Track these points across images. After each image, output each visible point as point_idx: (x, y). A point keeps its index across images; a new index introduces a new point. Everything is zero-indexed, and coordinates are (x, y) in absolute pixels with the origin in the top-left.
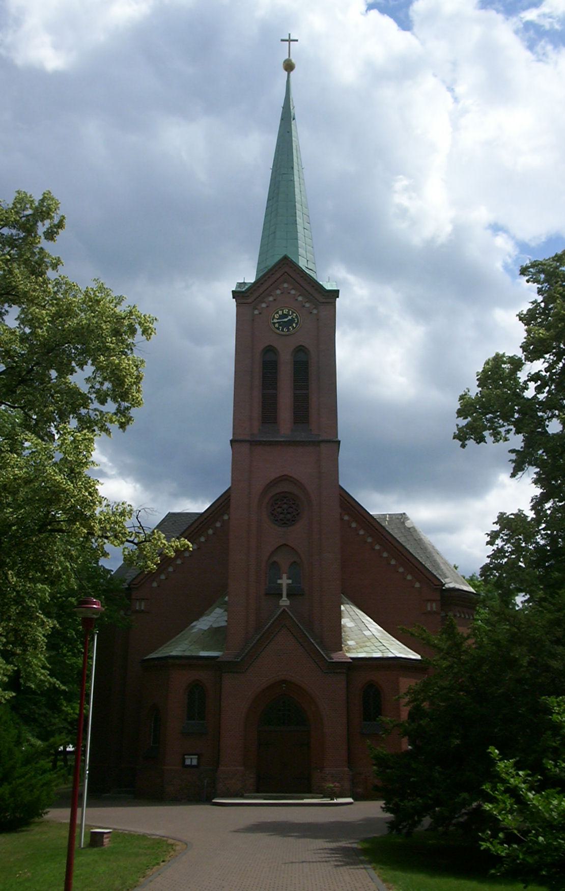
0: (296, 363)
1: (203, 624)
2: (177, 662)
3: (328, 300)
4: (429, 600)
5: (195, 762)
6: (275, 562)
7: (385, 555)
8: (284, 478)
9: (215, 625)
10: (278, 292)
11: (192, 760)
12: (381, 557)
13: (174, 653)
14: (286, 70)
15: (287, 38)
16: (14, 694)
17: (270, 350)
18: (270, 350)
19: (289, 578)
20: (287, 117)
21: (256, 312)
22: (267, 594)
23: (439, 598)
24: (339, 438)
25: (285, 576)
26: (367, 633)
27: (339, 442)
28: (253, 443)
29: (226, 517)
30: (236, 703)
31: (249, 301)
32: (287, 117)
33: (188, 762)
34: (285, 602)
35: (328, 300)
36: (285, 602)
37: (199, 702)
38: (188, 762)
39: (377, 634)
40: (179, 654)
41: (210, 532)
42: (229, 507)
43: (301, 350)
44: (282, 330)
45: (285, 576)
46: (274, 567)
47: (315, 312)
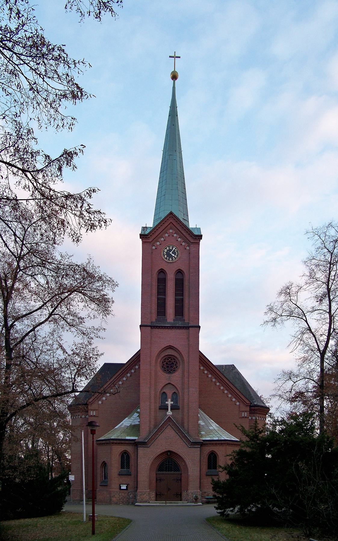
0: (176, 280)
1: (126, 422)
2: (115, 442)
3: (196, 241)
6: (164, 392)
8: (170, 347)
9: (133, 424)
10: (167, 235)
11: (124, 487)
15: (173, 55)
16: (239, 507)
18: (162, 271)
21: (154, 248)
22: (207, 475)
25: (169, 400)
26: (211, 428)
27: (199, 327)
29: (137, 367)
30: (146, 460)
31: (150, 240)
34: (169, 413)
35: (196, 241)
36: (169, 413)
37: (126, 460)
39: (216, 428)
40: (116, 438)
41: (129, 375)
42: (139, 361)
43: (179, 272)
44: (169, 260)
45: (169, 400)
47: (188, 248)
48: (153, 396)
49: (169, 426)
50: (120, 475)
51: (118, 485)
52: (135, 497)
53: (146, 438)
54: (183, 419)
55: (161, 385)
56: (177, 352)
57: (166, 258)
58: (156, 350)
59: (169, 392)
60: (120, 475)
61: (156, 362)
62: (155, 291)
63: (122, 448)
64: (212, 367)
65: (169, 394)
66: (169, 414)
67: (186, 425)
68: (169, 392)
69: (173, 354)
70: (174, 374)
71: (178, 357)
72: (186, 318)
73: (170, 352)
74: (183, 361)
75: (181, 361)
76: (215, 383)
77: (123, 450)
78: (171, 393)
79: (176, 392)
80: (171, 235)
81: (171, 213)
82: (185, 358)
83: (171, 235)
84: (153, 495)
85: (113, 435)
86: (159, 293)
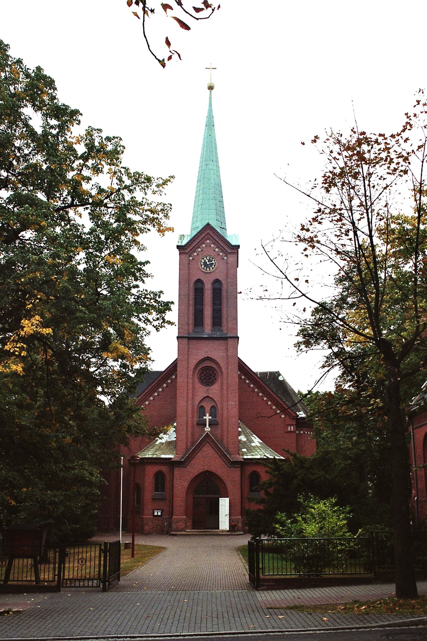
2: (150, 461)
4: (289, 425)
5: (159, 514)
6: (202, 406)
7: (265, 399)
10: (204, 246)
11: (158, 513)
12: (259, 395)
13: (147, 456)
14: (209, 89)
17: (199, 281)
19: (210, 416)
20: (210, 125)
21: (191, 258)
23: (295, 424)
24: (239, 335)
25: (207, 415)
26: (253, 444)
27: (238, 338)
28: (190, 338)
29: (174, 377)
30: (181, 482)
31: (187, 251)
32: (210, 125)
33: (156, 514)
34: (207, 429)
36: (207, 429)
37: (161, 481)
38: (156, 514)
43: (217, 281)
44: (206, 270)
45: (207, 415)
46: (201, 411)
47: (225, 258)
48: (190, 409)
49: (207, 444)
50: (154, 499)
51: (151, 511)
52: (170, 525)
53: (183, 458)
54: (222, 436)
55: (198, 399)
56: (216, 364)
57: (204, 269)
58: (193, 362)
59: (207, 406)
60: (154, 499)
61: (194, 372)
62: (192, 302)
63: (156, 468)
64: (253, 374)
65: (208, 408)
66: (207, 430)
67: (225, 441)
68: (207, 406)
69: (210, 365)
70: (211, 388)
71: (218, 370)
72: (224, 328)
73: (207, 364)
74: (221, 371)
75: (219, 373)
76: (258, 393)
77: (157, 470)
78: (209, 408)
79: (215, 405)
80: (208, 246)
81: (208, 224)
82: (223, 365)
83: (208, 246)
84: (190, 524)
85: (149, 454)
86: (196, 304)
